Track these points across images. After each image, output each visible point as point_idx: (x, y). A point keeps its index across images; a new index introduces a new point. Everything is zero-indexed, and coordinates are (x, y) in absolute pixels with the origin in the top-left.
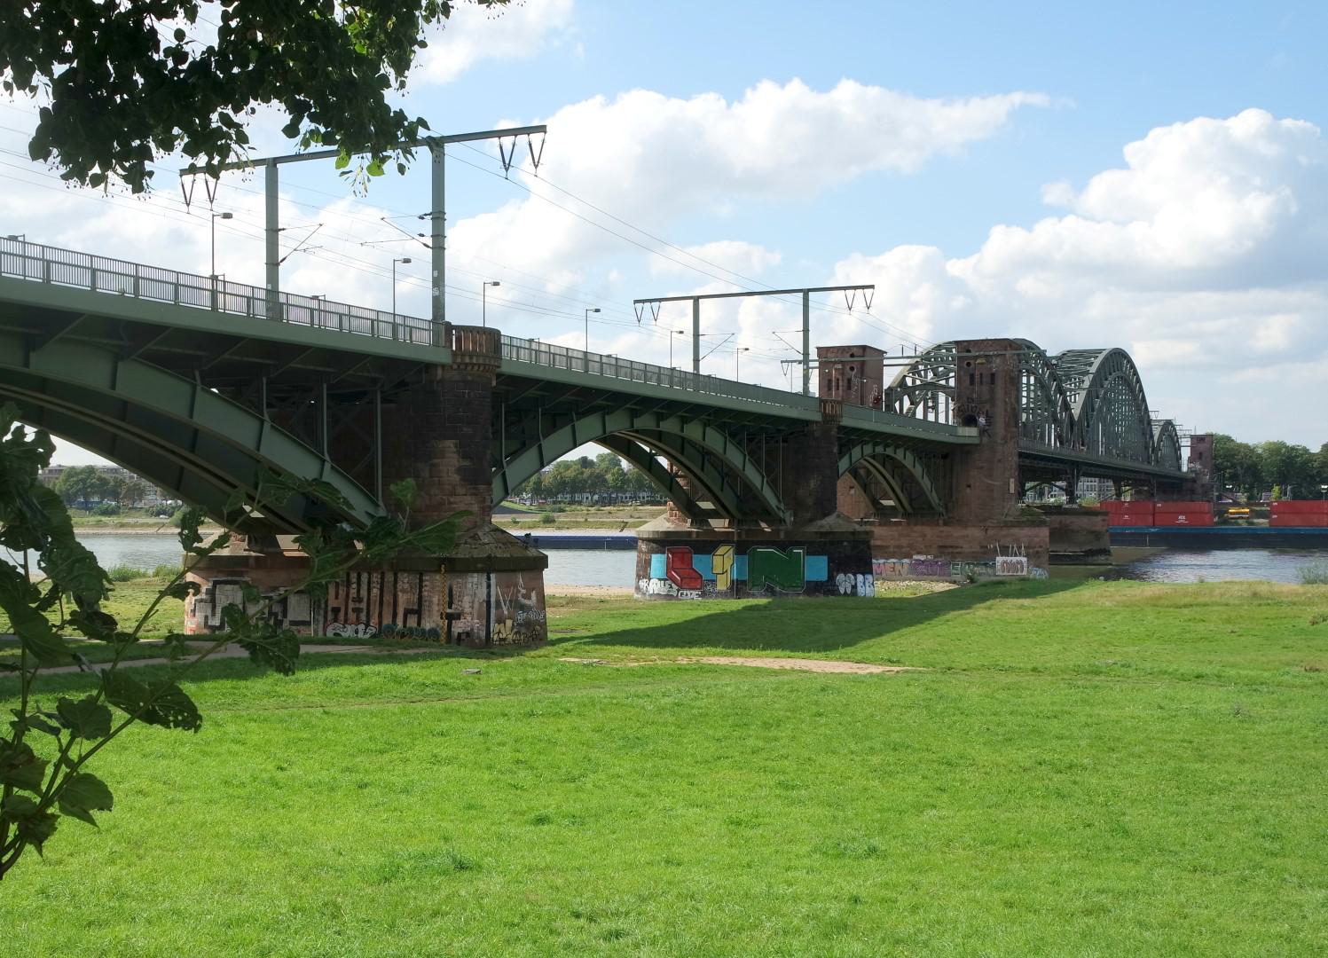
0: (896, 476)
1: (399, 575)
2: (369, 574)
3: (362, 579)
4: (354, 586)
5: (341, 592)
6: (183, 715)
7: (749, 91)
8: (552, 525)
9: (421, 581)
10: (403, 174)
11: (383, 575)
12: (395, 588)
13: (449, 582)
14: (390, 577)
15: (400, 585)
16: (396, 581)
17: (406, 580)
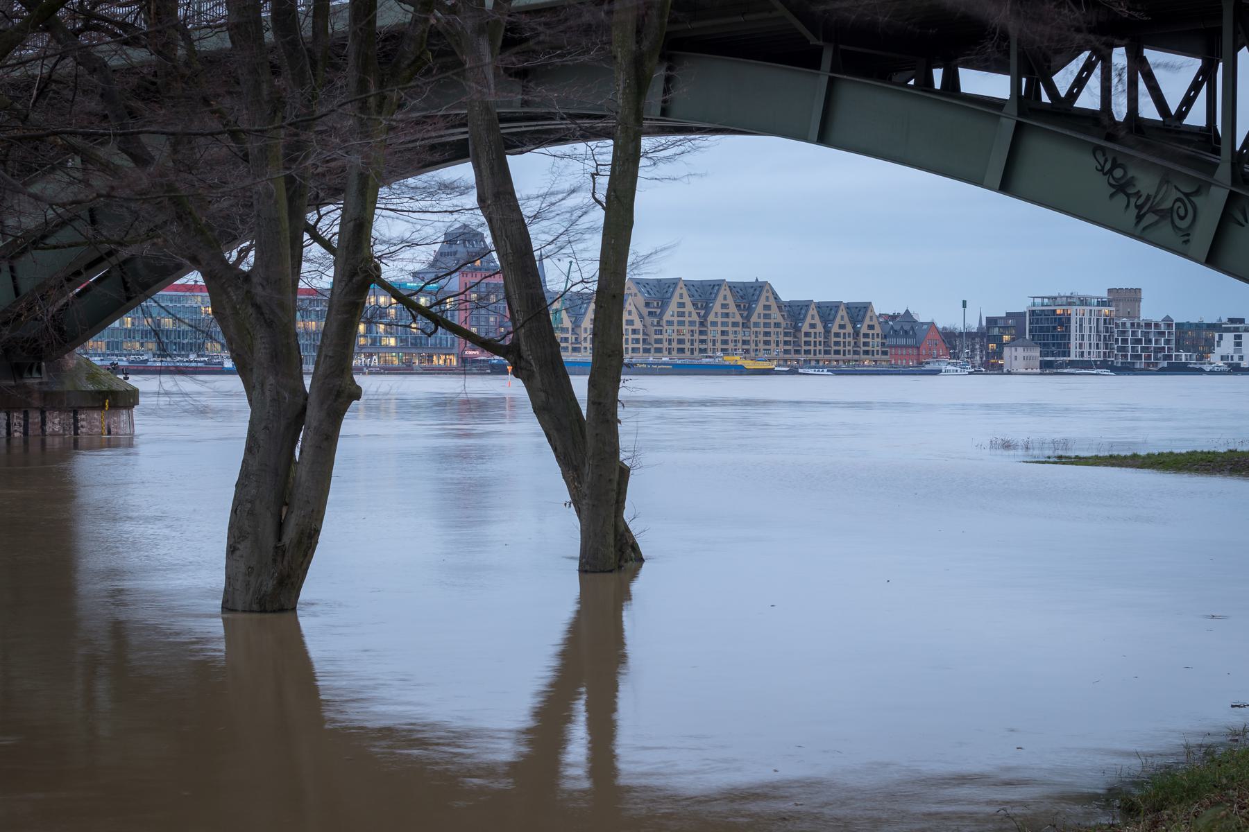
1: (47, 414)
6: (87, 6)
7: (617, 693)
8: (113, 69)
9: (76, 421)
11: (26, 414)
12: (43, 431)
13: (107, 421)
14: (35, 417)
15: (49, 428)
16: (43, 423)
17: (57, 421)
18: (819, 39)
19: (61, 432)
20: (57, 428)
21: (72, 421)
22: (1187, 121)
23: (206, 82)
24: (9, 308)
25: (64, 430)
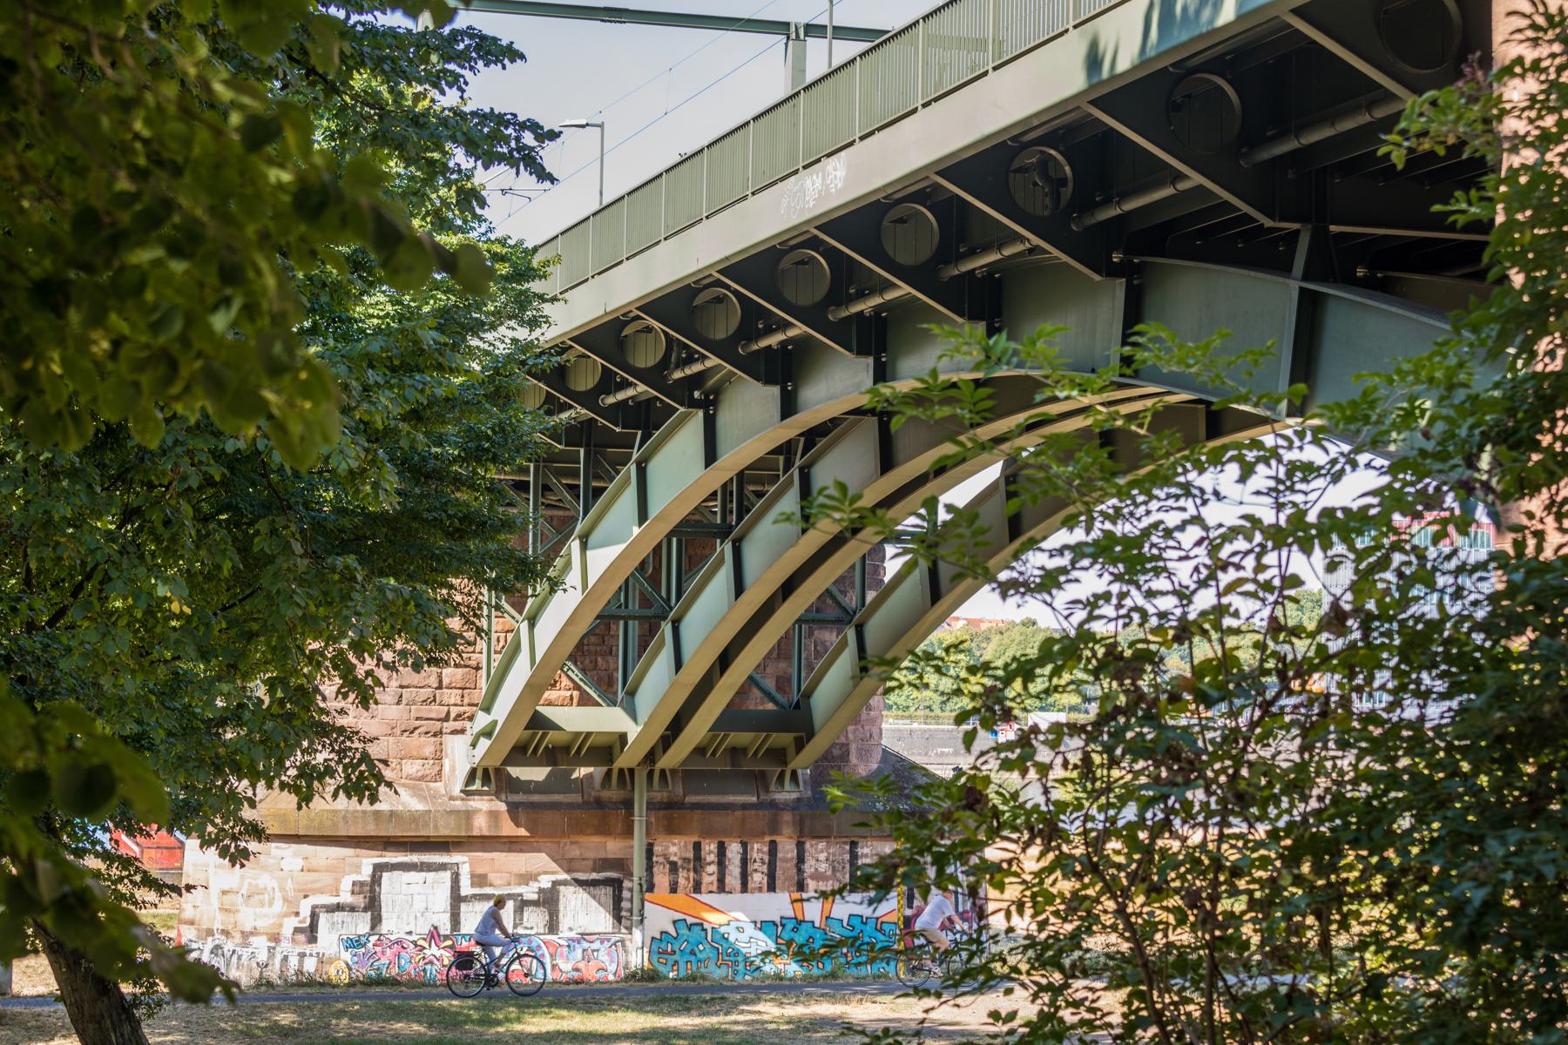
0: (1243, 522)
2: (744, 845)
3: (729, 854)
4: (713, 868)
5: (682, 881)
10: (522, 57)
12: (800, 871)
15: (809, 867)
16: (801, 859)
17: (822, 856)
18: (518, 825)
19: (829, 873)
20: (823, 867)
21: (847, 857)
22: (1541, 558)
23: (1193, 898)
24: (1363, 566)
25: (834, 870)
